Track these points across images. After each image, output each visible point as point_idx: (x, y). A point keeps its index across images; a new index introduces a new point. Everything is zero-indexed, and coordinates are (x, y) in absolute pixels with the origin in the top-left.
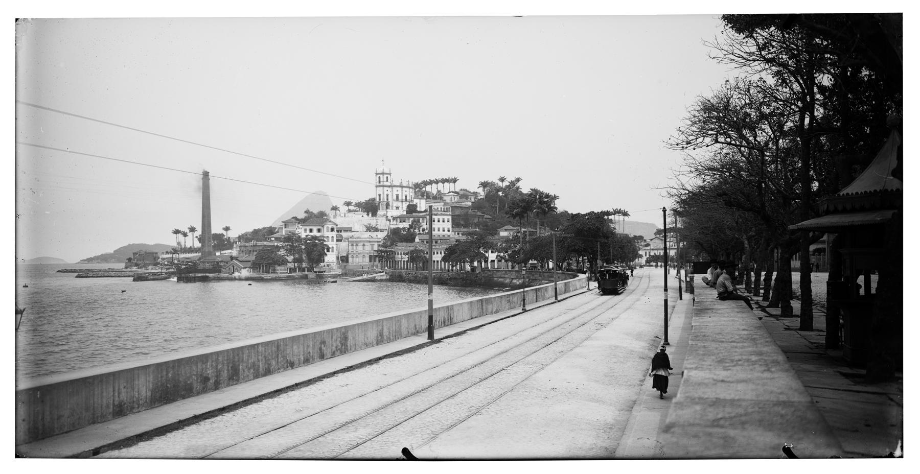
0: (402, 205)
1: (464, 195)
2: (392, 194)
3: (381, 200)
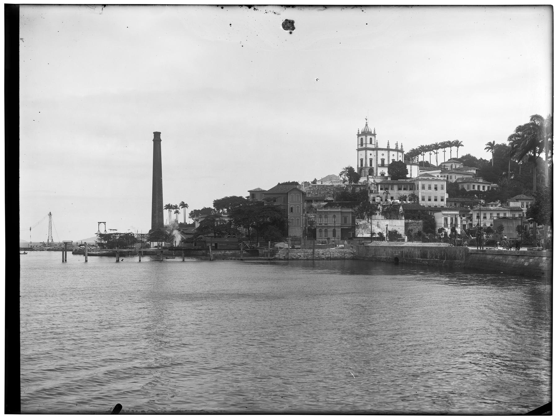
1: (468, 161)
2: (377, 158)
3: (364, 166)
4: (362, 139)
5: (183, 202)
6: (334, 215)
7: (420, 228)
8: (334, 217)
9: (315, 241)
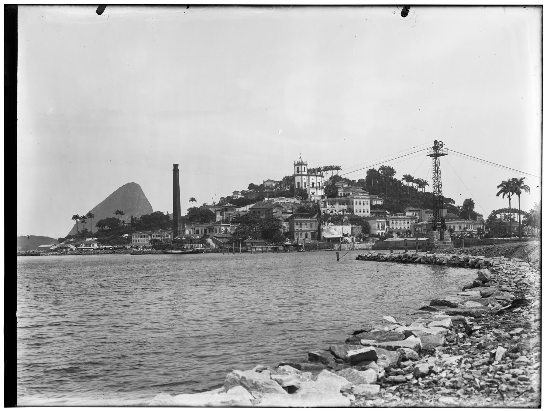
0: (317, 191)
4: (298, 168)
7: (360, 230)
8: (306, 224)
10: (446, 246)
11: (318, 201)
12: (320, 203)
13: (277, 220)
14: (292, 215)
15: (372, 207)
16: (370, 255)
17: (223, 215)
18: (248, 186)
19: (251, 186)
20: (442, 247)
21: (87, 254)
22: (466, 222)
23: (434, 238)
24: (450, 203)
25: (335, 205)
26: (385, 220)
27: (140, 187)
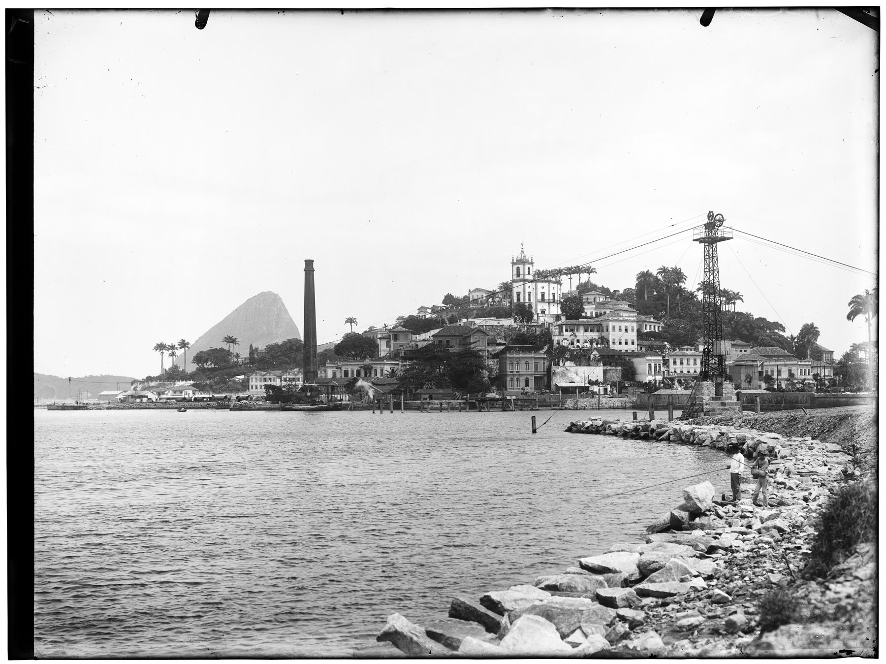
0: (549, 308)
4: (518, 268)
5: (184, 341)
6: (527, 362)
7: (619, 374)
8: (527, 363)
9: (505, 392)
10: (727, 410)
11: (549, 324)
12: (552, 328)
13: (476, 355)
14: (504, 347)
15: (640, 335)
16: (591, 423)
17: (390, 347)
18: (443, 298)
19: (449, 299)
20: (718, 412)
21: (165, 408)
22: (799, 363)
23: (703, 394)
24: (776, 331)
25: (577, 331)
26: (661, 358)
27: (280, 299)
